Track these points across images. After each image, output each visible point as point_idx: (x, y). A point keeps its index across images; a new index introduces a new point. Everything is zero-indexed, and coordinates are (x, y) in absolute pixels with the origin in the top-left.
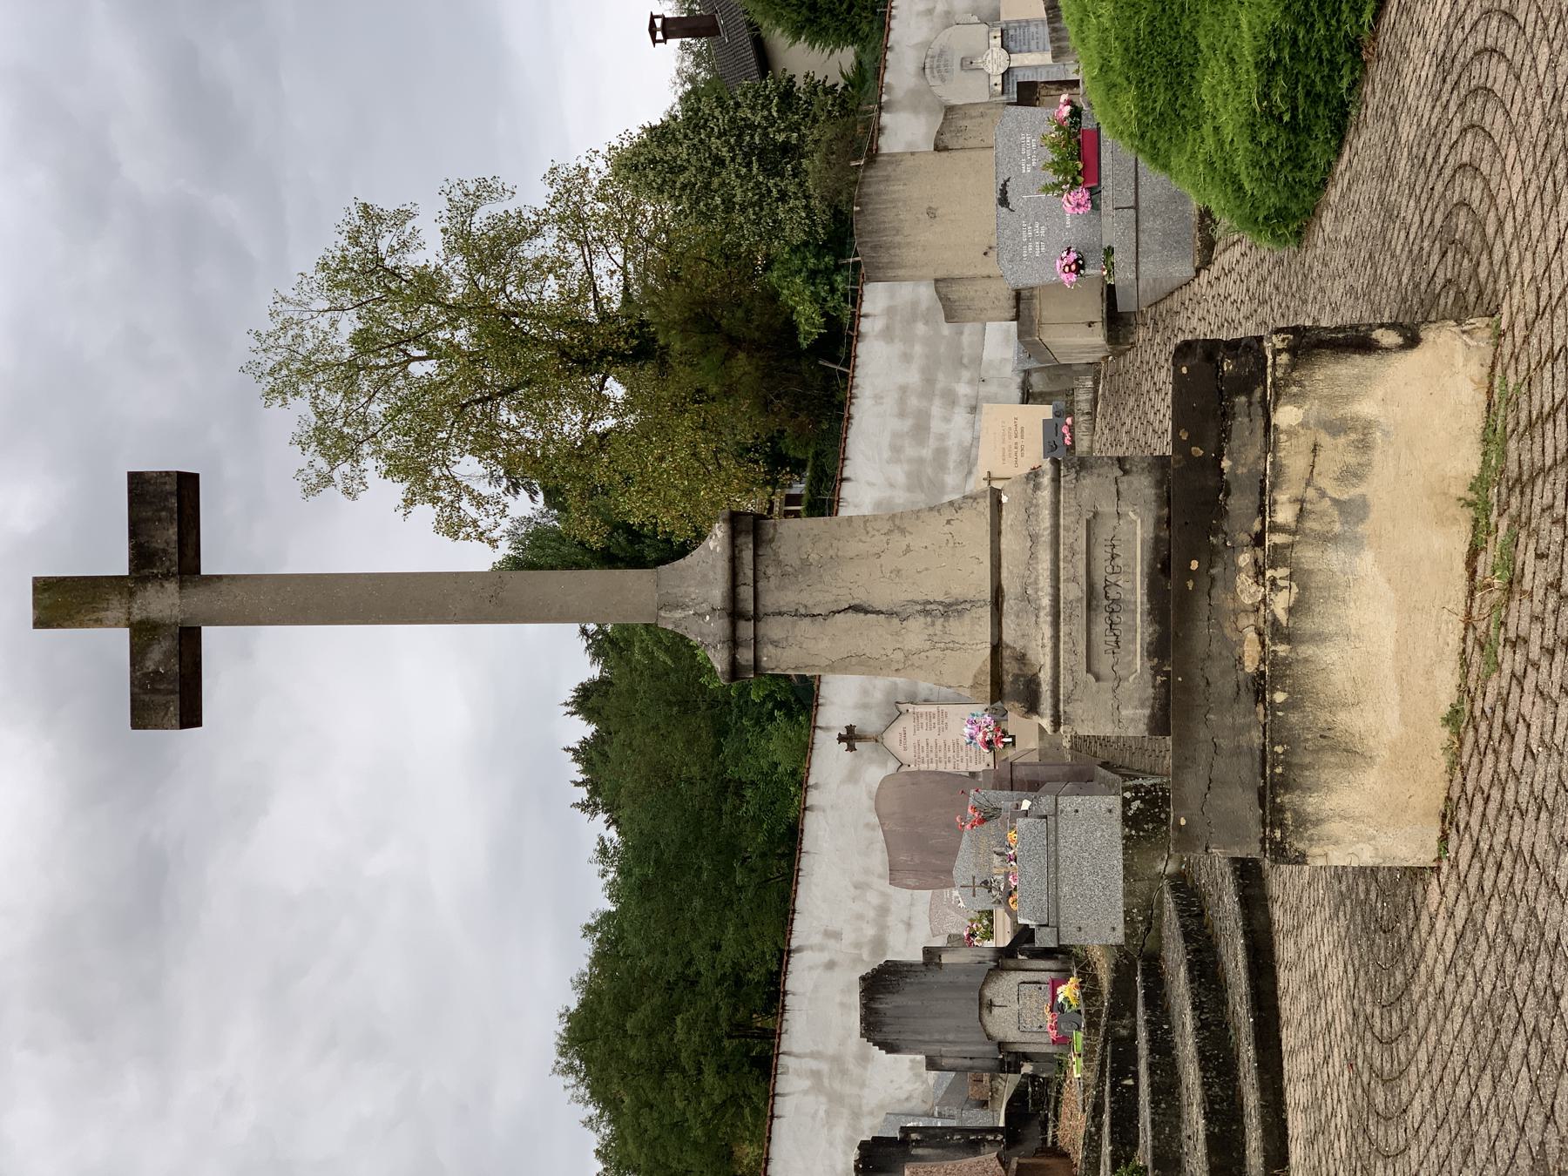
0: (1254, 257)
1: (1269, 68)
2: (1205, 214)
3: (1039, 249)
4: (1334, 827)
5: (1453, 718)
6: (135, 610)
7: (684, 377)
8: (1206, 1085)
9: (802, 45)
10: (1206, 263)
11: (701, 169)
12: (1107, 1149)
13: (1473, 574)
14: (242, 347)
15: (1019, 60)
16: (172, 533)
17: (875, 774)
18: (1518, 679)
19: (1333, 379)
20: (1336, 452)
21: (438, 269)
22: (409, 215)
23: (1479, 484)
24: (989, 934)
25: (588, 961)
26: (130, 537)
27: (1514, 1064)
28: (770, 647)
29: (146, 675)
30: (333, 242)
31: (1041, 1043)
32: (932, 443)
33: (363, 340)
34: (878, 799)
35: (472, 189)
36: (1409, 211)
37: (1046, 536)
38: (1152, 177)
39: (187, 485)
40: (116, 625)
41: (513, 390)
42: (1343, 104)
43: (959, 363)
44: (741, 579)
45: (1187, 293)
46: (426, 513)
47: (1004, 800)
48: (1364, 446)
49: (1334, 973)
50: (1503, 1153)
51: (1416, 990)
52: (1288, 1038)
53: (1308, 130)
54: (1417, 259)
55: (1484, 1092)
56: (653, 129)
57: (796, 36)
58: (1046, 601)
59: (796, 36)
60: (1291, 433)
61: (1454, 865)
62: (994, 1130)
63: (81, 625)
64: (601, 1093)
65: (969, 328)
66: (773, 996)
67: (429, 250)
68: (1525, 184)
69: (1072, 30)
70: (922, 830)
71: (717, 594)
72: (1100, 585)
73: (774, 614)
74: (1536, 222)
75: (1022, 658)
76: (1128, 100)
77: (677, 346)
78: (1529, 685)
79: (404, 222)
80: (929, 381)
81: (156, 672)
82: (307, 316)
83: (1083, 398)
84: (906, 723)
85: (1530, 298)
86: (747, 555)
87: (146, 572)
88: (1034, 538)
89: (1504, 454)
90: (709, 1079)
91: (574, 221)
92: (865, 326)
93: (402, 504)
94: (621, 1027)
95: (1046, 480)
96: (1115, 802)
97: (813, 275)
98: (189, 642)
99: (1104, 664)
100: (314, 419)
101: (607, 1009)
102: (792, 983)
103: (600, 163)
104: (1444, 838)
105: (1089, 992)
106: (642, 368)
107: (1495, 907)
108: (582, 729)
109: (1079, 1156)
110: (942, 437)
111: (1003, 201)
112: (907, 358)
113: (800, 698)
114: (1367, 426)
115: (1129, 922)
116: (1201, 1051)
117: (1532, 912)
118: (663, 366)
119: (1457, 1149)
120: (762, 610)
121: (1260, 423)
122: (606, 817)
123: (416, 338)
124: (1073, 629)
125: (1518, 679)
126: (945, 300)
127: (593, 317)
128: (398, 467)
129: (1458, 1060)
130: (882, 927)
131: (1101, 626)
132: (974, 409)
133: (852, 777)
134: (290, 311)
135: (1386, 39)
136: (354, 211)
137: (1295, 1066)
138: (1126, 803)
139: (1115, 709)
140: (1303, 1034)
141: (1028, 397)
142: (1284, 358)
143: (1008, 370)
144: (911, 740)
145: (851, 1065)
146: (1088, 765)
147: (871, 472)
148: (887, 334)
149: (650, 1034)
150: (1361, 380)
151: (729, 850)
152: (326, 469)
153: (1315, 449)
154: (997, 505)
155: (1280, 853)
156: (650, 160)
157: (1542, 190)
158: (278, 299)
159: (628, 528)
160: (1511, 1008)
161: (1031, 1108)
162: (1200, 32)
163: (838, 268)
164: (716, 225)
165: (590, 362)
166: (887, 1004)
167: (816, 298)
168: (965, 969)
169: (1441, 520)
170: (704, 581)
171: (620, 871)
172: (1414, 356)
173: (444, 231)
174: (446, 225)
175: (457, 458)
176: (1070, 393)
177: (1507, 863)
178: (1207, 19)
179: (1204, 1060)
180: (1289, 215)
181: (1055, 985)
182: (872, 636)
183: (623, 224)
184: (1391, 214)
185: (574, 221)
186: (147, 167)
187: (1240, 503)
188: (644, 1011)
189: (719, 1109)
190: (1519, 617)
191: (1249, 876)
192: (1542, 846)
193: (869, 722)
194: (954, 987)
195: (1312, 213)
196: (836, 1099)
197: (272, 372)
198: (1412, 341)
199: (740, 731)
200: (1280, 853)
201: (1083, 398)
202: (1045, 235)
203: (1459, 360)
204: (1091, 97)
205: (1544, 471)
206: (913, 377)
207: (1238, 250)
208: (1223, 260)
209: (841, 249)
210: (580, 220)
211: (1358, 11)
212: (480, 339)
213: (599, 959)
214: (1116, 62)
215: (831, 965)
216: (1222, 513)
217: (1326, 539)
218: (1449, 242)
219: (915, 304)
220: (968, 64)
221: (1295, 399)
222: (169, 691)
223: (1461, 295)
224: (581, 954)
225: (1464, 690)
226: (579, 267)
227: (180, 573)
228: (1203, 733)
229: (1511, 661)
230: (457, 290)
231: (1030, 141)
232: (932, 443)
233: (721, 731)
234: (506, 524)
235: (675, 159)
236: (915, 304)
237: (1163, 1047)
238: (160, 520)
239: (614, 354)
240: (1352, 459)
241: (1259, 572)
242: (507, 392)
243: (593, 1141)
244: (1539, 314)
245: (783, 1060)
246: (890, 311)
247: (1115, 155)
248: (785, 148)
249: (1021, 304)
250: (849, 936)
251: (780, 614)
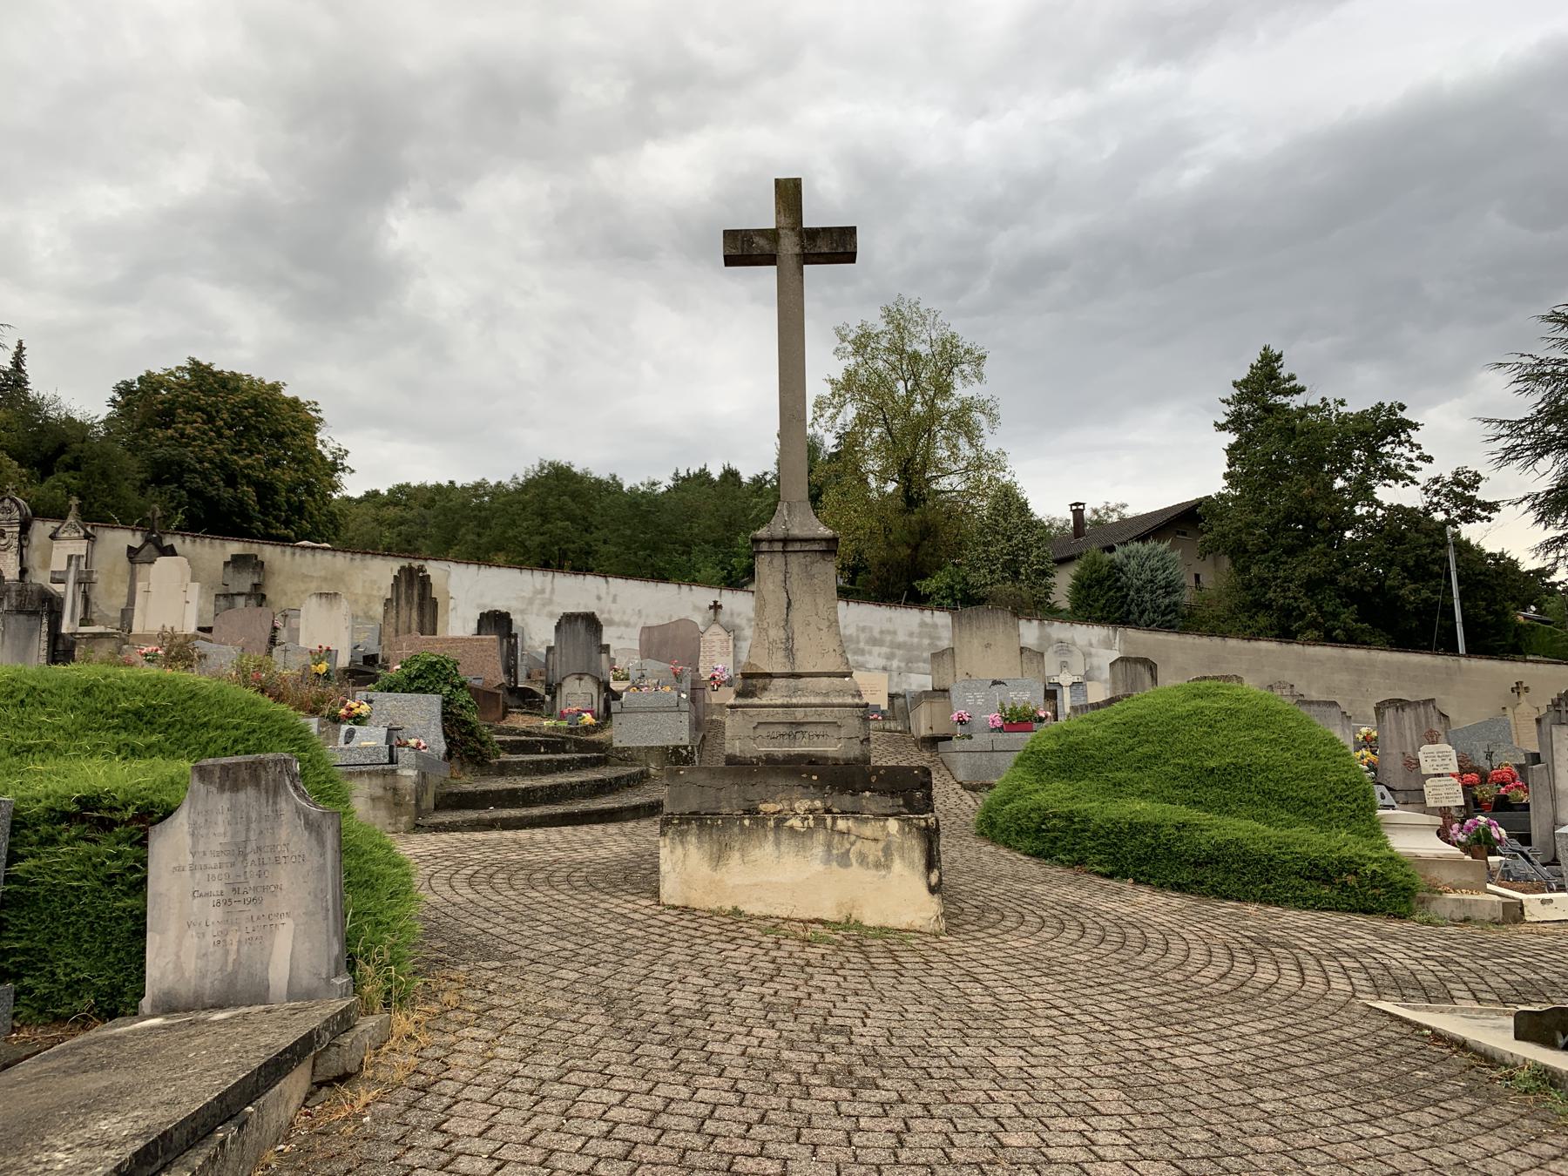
0: (970, 812)
1: (1069, 818)
2: (991, 786)
3: (970, 702)
4: (679, 851)
5: (736, 911)
7: (898, 522)
8: (542, 788)
9: (1071, 581)
10: (965, 787)
12: (508, 738)
13: (812, 922)
14: (912, 295)
15: (1067, 691)
16: (825, 250)
17: (698, 619)
18: (759, 945)
19: (912, 848)
20: (874, 851)
22: (980, 380)
23: (859, 925)
24: (616, 679)
27: (560, 943)
30: (966, 341)
31: (562, 704)
32: (867, 648)
33: (915, 357)
34: (686, 621)
36: (997, 890)
37: (828, 701)
38: (1012, 758)
39: (850, 257)
42: (1051, 856)
43: (909, 661)
45: (949, 777)
46: (827, 390)
47: (687, 685)
48: (878, 865)
49: (602, 852)
50: (514, 938)
51: (596, 894)
52: (567, 830)
53: (1037, 838)
54: (973, 894)
55: (544, 928)
57: (1076, 578)
58: (794, 701)
59: (1076, 578)
60: (884, 828)
61: (661, 913)
62: (516, 682)
64: (530, 484)
65: (927, 667)
66: (580, 569)
67: (962, 390)
68: (1015, 948)
69: (1087, 716)
70: (668, 643)
71: (796, 532)
72: (803, 729)
74: (997, 954)
75: (765, 689)
76: (1051, 745)
78: (756, 950)
80: (899, 646)
83: (892, 725)
84: (724, 635)
85: (957, 951)
86: (816, 547)
88: (827, 694)
89: (875, 938)
90: (538, 539)
91: (978, 464)
92: (928, 613)
95: (857, 700)
96: (686, 742)
97: (951, 588)
98: (769, 259)
99: (762, 731)
101: (572, 487)
102: (589, 578)
103: (1008, 478)
104: (675, 908)
105: (587, 729)
107: (640, 934)
108: (716, 474)
109: (504, 724)
110: (870, 653)
111: (995, 683)
112: (911, 634)
113: (738, 578)
114: (888, 867)
115: (624, 749)
116: (559, 785)
117: (639, 952)
118: (904, 511)
119: (515, 915)
121: (889, 811)
123: (917, 384)
124: (781, 715)
125: (759, 945)
126: (943, 652)
127: (928, 475)
128: (850, 376)
129: (561, 915)
130: (619, 625)
131: (783, 729)
132: (885, 669)
133: (696, 608)
134: (930, 320)
135: (1086, 878)
137: (554, 834)
138: (685, 747)
139: (739, 738)
140: (570, 837)
141: (892, 697)
142: (923, 824)
143: (905, 687)
144: (715, 638)
145: (548, 609)
146: (705, 727)
147: (858, 617)
148: (923, 624)
149: (560, 509)
150: (912, 864)
151: (655, 548)
153: (876, 840)
154: (844, 675)
155: (666, 823)
156: (1010, 503)
157: (1013, 957)
159: (820, 495)
160: (588, 942)
161: (527, 700)
162: (1087, 782)
163: (955, 601)
164: (976, 537)
166: (580, 626)
167: (939, 589)
168: (599, 665)
169: (840, 905)
170: (802, 525)
172: (925, 891)
176: (895, 719)
177: (663, 940)
178: (1094, 785)
179: (555, 787)
180: (991, 829)
181: (591, 712)
182: (775, 612)
183: (976, 491)
184: (995, 880)
185: (978, 464)
186: (1004, 245)
187: (847, 800)
188: (572, 505)
189: (522, 544)
190: (790, 945)
191: (652, 810)
192: (674, 957)
193: (724, 617)
194: (590, 661)
195: (994, 841)
196: (531, 601)
198: (933, 890)
199: (716, 554)
200: (666, 823)
201: (892, 725)
202: (977, 704)
203: (924, 914)
204: (1051, 726)
205: (867, 958)
206: (901, 638)
207: (972, 803)
208: (967, 796)
209: (964, 600)
210: (979, 467)
211: (1100, 863)
213: (599, 482)
214: (1071, 738)
215: (599, 598)
216: (842, 792)
217: (829, 846)
218: (983, 910)
219: (939, 638)
220: (1064, 665)
221: (901, 829)
222: (743, 249)
223: (956, 916)
225: (752, 917)
226: (954, 467)
228: (728, 782)
229: (768, 941)
230: (941, 405)
231: (1026, 696)
232: (867, 648)
233: (716, 544)
234: (821, 432)
236: (939, 638)
237: (561, 767)
240: (871, 858)
241: (811, 811)
243: (506, 480)
244: (949, 955)
245: (550, 575)
246: (935, 626)
247: (1022, 740)
248: (1017, 573)
249: (941, 692)
250: (613, 607)
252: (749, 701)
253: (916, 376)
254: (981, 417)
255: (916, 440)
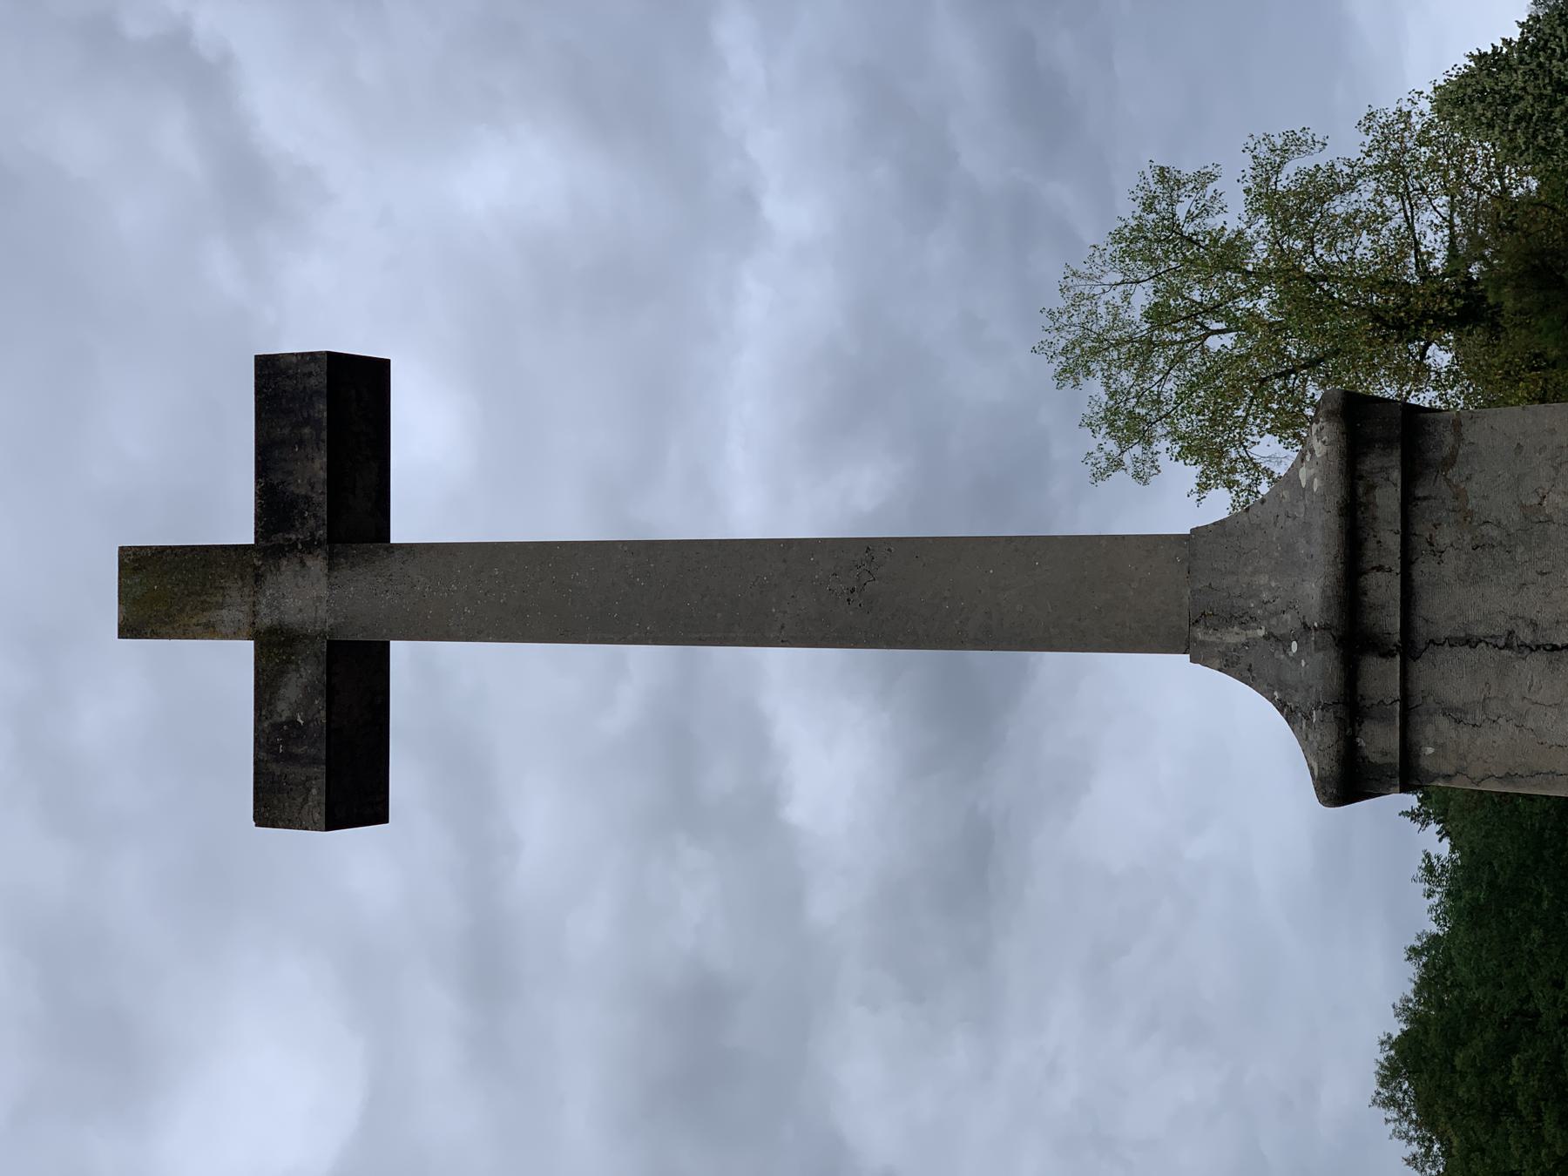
6: (263, 609)
11: (1539, 98)
16: (318, 466)
21: (1240, 233)
22: (1212, 177)
25: (1413, 986)
26: (258, 475)
28: (1444, 723)
29: (277, 727)
30: (1127, 210)
33: (1158, 315)
35: (1279, 143)
40: (235, 636)
41: (1318, 361)
44: (1371, 555)
56: (1483, 56)
63: (185, 634)
67: (1232, 214)
73: (1453, 642)
77: (1509, 304)
79: (1204, 186)
81: (292, 722)
82: (1098, 290)
86: (1387, 499)
87: (279, 538)
93: (1195, 488)
94: (1448, 1060)
100: (1106, 398)
103: (1425, 106)
106: (1470, 333)
118: (1495, 329)
120: (1422, 631)
122: (1438, 827)
123: (1214, 310)
128: (1192, 449)
134: (1082, 286)
136: (1148, 175)
152: (1116, 451)
158: (1069, 273)
165: (1408, 327)
171: (1449, 894)
173: (1247, 191)
174: (1250, 184)
175: (1256, 438)
185: (1394, 169)
197: (1065, 351)
212: (1281, 306)
213: (1423, 985)
222: (325, 760)
224: (1403, 979)
226: (1398, 220)
227: (332, 539)
235: (1508, 88)
238: (301, 443)
239: (1436, 317)
242: (1312, 364)
251: (1470, 642)
253: (1196, 312)
254: (1290, 169)
255: (1333, 306)
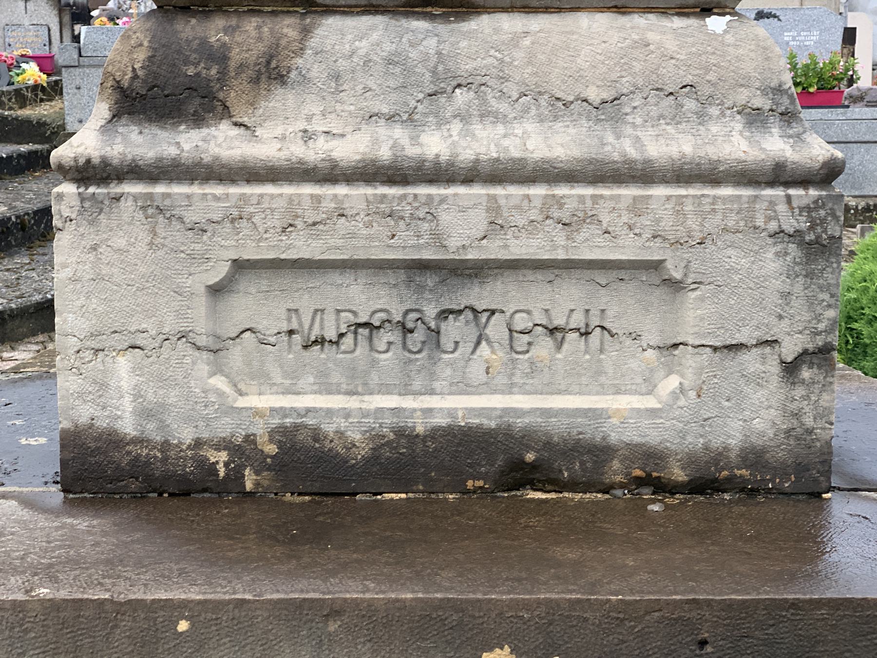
58: (434, 145)
72: (479, 295)
75: (272, 72)
88: (610, 109)
99: (251, 306)
124: (359, 224)
131: (365, 298)
252: (186, 142)
